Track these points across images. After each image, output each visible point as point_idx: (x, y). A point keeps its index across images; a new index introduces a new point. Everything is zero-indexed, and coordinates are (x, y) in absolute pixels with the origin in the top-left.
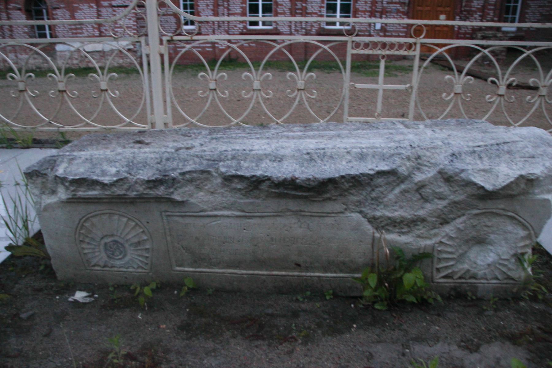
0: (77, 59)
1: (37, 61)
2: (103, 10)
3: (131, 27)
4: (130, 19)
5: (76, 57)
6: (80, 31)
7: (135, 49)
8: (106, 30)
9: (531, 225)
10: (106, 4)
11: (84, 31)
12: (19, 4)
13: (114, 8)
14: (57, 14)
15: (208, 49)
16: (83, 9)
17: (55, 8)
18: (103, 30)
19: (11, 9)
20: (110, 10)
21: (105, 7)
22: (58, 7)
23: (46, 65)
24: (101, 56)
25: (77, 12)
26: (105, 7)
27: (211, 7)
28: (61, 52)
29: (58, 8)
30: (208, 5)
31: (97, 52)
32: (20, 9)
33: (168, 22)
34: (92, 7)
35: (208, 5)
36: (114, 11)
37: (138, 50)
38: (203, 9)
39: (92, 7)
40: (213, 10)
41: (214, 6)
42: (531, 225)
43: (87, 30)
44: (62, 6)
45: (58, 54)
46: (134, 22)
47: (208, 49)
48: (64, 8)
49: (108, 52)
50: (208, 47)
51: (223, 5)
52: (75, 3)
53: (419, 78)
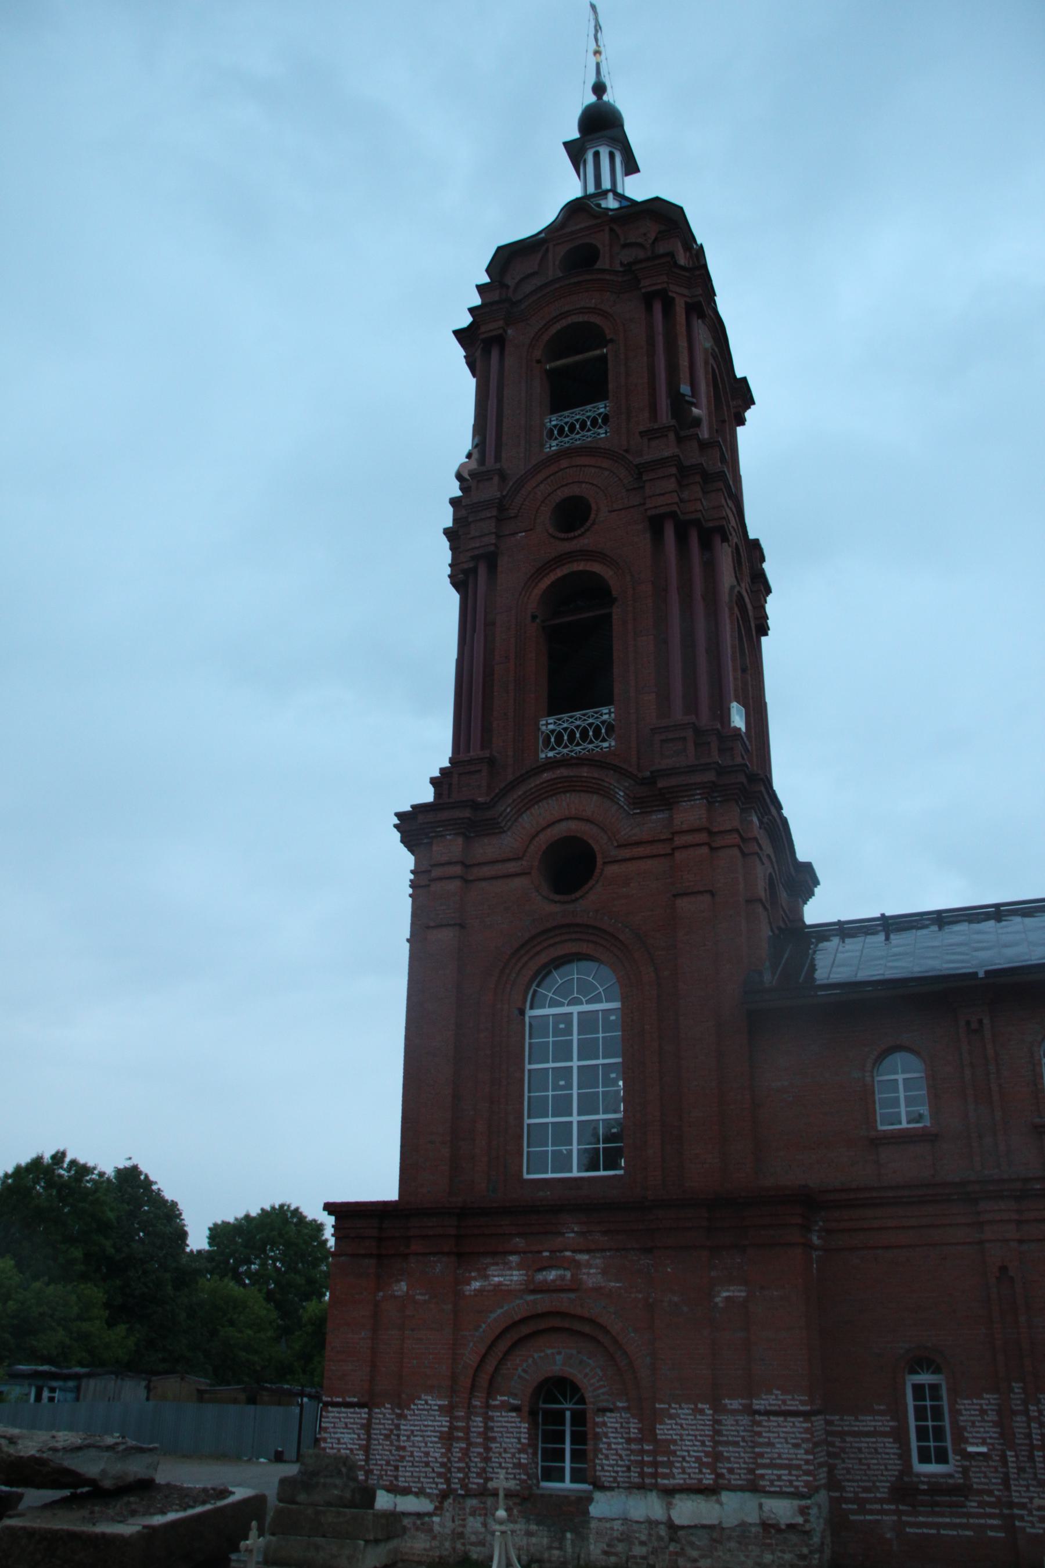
0: (643, 1543)
1: (534, 1540)
2: (728, 1420)
3: (798, 1467)
4: (796, 1446)
5: (644, 1538)
6: (667, 1471)
7: (807, 1527)
8: (731, 1471)
9: (575, 537)
10: (735, 1404)
11: (675, 1471)
12: (515, 1396)
13: (758, 1418)
14: (604, 1424)
15: (991, 1534)
16: (678, 1415)
17: (604, 1410)
18: (724, 1471)
19: (496, 1408)
20: (745, 1420)
21: (734, 1412)
22: (612, 1406)
23: (556, 1552)
24: (714, 1540)
25: (662, 1423)
26: (734, 1412)
27: (992, 1416)
28: (600, 1520)
29: (611, 1411)
30: (983, 1412)
31: (704, 1527)
32: (516, 1409)
33: (877, 1452)
34: (702, 1412)
35: (983, 1412)
36: (759, 1424)
37: (814, 1529)
38: (973, 1422)
39: (702, 1412)
40: (996, 1424)
41: (999, 1412)
42: (575, 537)
43: (683, 1468)
44: (619, 1404)
45: (593, 1524)
46: (807, 1452)
47: (991, 1534)
48: (627, 1409)
49: (732, 1529)
50: (992, 1527)
51: (1026, 1412)
52: (661, 1402)
53: (566, 1493)
